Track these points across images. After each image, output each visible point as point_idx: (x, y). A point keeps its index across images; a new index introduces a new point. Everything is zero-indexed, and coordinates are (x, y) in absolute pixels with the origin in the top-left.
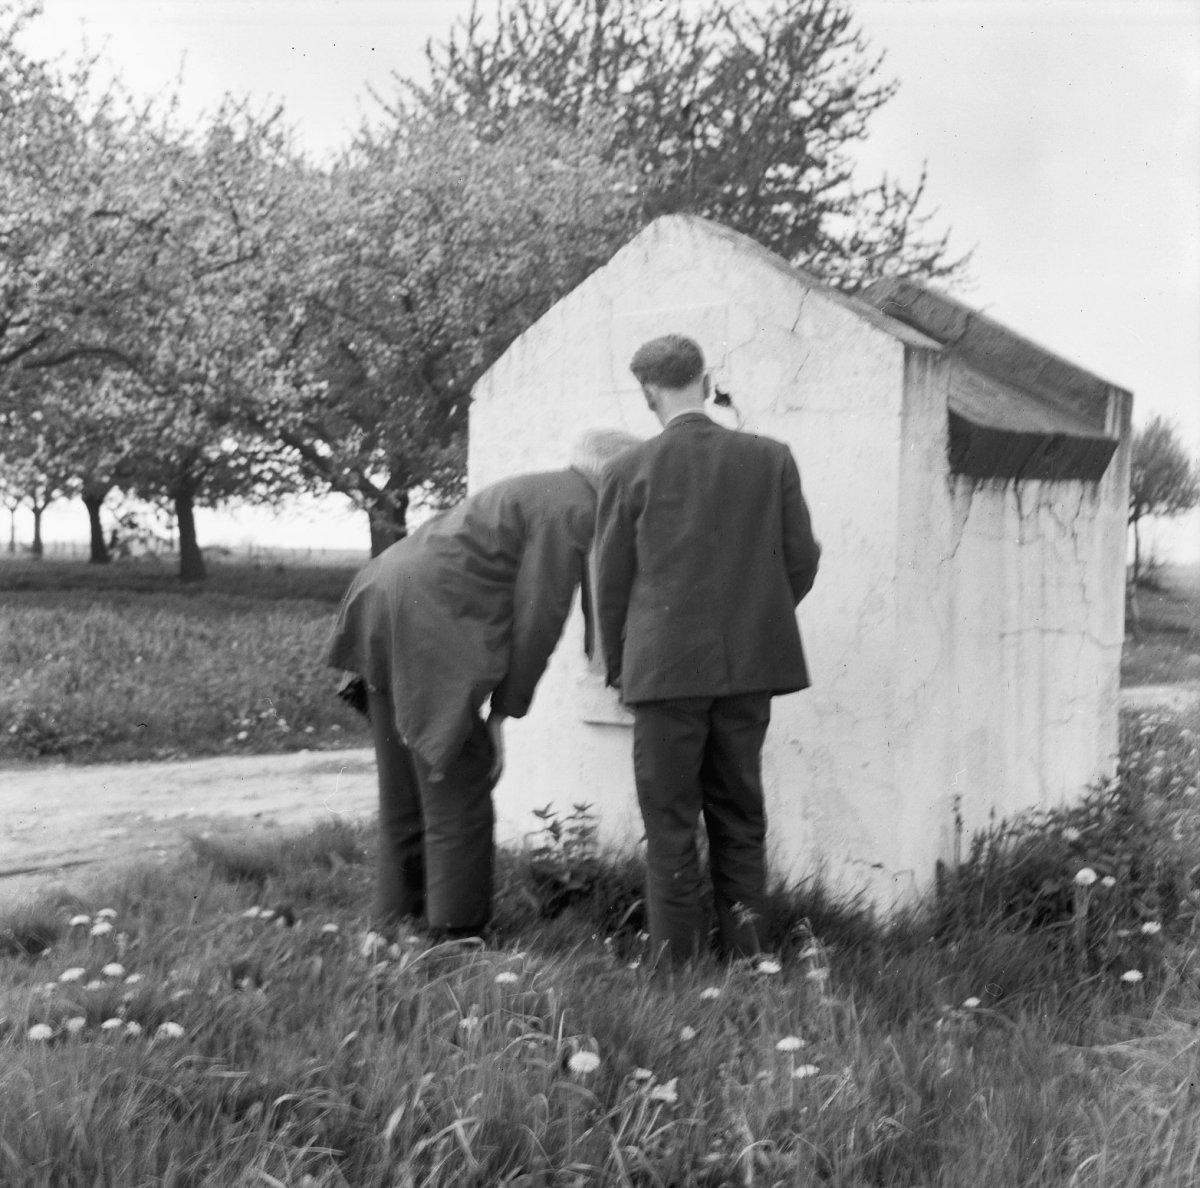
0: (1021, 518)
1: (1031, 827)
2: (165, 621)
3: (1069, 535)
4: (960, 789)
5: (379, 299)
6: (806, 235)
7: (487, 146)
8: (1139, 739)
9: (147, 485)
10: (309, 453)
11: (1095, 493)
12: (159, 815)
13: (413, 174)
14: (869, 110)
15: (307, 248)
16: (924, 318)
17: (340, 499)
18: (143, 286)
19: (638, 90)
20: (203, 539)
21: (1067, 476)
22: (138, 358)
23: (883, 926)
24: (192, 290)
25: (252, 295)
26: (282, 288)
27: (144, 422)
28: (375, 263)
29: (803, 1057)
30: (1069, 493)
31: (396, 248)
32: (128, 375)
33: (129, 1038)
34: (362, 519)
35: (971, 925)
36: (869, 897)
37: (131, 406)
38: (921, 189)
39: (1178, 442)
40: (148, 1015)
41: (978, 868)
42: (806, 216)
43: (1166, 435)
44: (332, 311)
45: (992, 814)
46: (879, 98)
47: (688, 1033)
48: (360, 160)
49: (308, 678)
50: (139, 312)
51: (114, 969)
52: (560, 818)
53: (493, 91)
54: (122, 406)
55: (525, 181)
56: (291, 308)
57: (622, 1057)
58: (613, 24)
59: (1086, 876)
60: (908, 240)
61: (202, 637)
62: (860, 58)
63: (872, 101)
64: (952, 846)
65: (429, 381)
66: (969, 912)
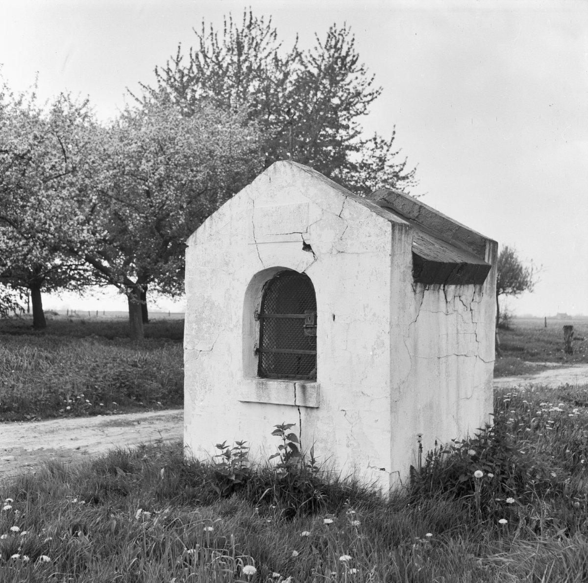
0: (447, 302)
1: (454, 449)
2: (27, 350)
3: (469, 309)
4: (421, 431)
5: (133, 191)
6: (340, 160)
7: (187, 118)
8: (502, 405)
9: (17, 281)
10: (98, 266)
11: (480, 290)
12: (29, 449)
13: (151, 132)
14: (368, 102)
15: (99, 167)
16: (399, 208)
17: (112, 289)
18: (19, 187)
19: (258, 91)
20: (46, 306)
21: (468, 283)
22: (16, 221)
23: (386, 498)
24: (42, 188)
25: (71, 190)
26: (86, 186)
27: (17, 251)
28: (132, 174)
29: (352, 565)
30: (468, 291)
31: (143, 167)
32: (11, 229)
33: (26, 563)
34: (124, 297)
35: (428, 497)
36: (379, 485)
37: (11, 244)
38: (393, 138)
39: (516, 259)
40: (34, 552)
41: (430, 469)
42: (339, 152)
43: (511, 256)
44: (111, 197)
45: (436, 443)
46: (373, 96)
47: (295, 553)
48: (123, 124)
49: (101, 379)
50: (16, 199)
51: (15, 528)
52: (230, 448)
53: (188, 91)
54: (6, 243)
55: (205, 135)
56: (91, 196)
57: (265, 567)
58: (245, 60)
59: (479, 473)
60: (387, 163)
61: (47, 358)
62: (363, 77)
63: (369, 98)
64: (417, 457)
65: (159, 231)
66: (426, 491)
